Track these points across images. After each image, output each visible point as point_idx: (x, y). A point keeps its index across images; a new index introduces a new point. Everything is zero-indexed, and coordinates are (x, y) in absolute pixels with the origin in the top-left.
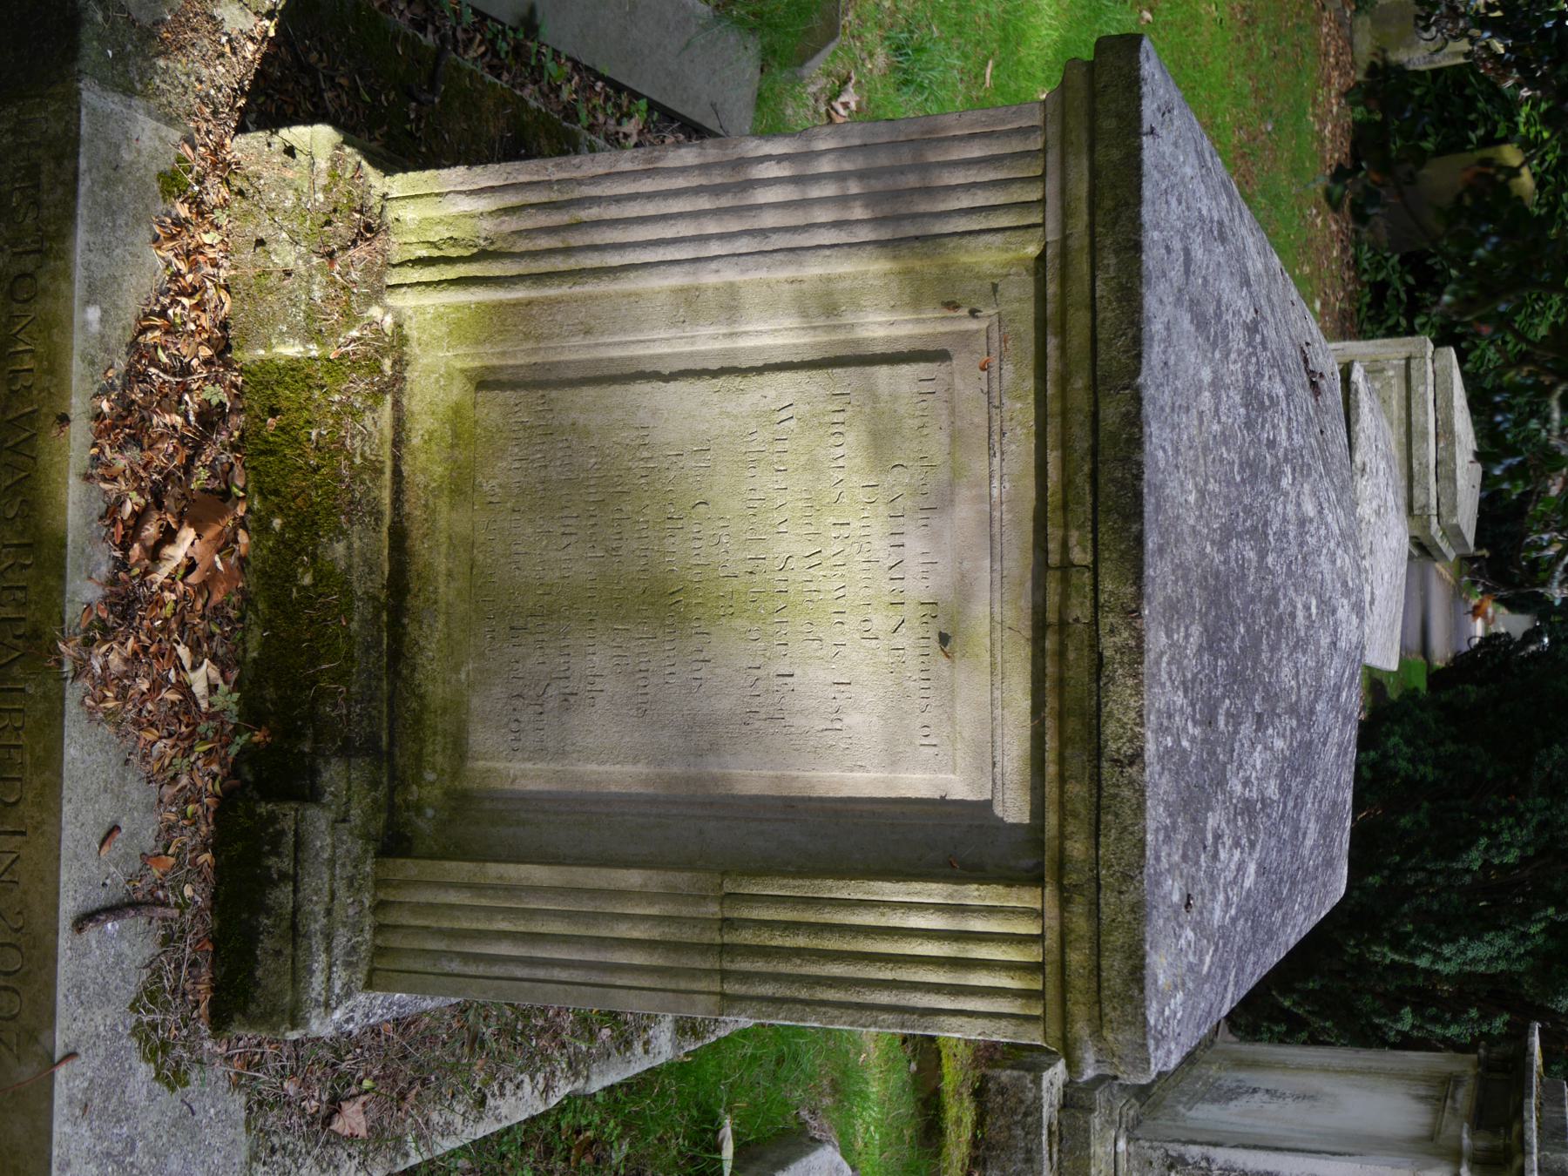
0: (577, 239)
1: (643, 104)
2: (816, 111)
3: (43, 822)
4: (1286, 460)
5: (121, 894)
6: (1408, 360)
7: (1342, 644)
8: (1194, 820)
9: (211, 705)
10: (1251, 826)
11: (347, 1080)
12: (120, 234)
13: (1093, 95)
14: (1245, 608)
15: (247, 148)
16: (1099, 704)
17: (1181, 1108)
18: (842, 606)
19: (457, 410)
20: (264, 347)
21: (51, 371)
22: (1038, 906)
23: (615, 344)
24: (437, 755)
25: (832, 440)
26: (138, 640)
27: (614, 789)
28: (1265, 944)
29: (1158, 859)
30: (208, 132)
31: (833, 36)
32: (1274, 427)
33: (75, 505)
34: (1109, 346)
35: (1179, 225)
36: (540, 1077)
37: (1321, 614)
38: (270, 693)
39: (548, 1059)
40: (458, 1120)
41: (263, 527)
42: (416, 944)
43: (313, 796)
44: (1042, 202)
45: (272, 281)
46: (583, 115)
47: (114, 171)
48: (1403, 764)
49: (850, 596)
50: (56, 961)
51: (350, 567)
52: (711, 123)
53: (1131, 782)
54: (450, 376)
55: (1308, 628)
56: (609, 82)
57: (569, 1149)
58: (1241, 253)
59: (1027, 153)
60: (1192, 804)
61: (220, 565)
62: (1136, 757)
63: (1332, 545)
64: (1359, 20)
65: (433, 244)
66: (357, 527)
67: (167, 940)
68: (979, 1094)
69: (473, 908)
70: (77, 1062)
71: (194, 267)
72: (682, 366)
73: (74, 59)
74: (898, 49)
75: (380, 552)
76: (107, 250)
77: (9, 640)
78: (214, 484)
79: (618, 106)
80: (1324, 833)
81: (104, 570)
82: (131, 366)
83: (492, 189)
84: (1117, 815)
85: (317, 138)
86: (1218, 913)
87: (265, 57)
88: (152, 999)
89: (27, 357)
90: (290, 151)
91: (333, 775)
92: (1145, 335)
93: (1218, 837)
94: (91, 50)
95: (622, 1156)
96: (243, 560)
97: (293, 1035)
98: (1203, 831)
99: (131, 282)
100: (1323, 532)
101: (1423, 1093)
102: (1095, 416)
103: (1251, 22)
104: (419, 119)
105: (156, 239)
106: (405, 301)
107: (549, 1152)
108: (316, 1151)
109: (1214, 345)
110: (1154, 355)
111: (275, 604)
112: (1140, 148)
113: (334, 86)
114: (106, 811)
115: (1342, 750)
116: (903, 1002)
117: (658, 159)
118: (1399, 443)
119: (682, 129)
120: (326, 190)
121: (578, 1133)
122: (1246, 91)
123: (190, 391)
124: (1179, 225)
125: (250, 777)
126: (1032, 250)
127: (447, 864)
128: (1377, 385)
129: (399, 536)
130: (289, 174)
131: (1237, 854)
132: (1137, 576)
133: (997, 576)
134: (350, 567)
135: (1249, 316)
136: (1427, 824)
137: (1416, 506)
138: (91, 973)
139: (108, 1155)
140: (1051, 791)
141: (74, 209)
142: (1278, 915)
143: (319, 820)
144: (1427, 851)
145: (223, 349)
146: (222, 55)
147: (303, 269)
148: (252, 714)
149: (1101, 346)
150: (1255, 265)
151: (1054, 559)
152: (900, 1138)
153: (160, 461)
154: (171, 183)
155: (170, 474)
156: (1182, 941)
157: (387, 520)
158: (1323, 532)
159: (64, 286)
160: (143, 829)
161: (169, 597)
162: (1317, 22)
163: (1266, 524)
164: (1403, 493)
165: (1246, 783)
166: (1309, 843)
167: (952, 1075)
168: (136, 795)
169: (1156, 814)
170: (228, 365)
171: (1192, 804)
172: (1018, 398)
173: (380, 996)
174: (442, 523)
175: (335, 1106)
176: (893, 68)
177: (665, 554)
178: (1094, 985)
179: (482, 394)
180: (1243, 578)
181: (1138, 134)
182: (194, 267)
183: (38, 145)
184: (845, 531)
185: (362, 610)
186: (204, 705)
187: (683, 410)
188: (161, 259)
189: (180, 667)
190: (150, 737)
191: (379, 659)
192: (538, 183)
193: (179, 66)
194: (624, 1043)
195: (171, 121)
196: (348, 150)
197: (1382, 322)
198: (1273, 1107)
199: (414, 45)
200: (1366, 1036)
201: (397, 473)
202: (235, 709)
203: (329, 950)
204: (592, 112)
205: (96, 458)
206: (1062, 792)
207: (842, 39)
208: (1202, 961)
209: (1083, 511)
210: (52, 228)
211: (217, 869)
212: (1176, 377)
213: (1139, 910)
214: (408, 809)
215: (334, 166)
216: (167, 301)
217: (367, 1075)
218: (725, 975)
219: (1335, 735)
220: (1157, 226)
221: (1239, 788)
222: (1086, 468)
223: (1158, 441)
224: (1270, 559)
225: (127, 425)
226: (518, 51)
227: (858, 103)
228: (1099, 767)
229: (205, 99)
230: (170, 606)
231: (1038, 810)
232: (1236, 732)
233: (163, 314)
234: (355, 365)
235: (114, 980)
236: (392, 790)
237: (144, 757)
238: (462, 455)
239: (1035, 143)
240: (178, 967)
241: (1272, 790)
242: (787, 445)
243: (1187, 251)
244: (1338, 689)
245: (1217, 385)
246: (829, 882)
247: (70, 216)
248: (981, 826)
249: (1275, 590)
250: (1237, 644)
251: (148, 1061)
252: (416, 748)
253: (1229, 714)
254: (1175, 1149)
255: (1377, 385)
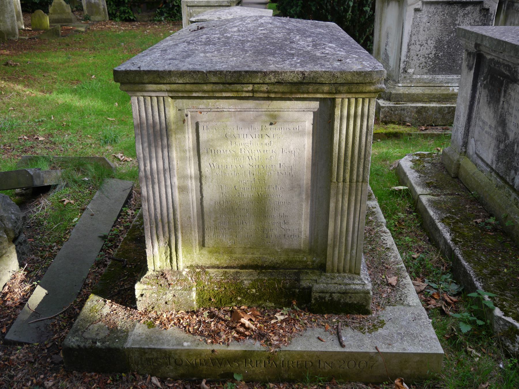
0: (166, 220)
1: (124, 209)
2: (123, 164)
3: (317, 356)
4: (223, 35)
5: (335, 336)
6: (188, 6)
7: (271, 21)
8: (318, 59)
9: (286, 315)
10: (319, 45)
11: (383, 282)
12: (164, 338)
13: (130, 83)
14: (262, 45)
15: (141, 306)
16: (289, 83)
17: (390, 69)
18: (264, 149)
19: (210, 252)
20: (193, 302)
21: (201, 355)
22: (341, 99)
23: (193, 210)
24: (300, 257)
25: (219, 153)
26: (270, 333)
27: (309, 211)
28: (349, 42)
29: (329, 68)
30: (137, 316)
31: (104, 159)
32: (214, 38)
33: (235, 347)
34: (195, 79)
35: (163, 61)
36: (382, 234)
37: (263, 26)
38: (283, 300)
39: (377, 232)
40: (393, 254)
41: (240, 302)
42: (348, 262)
43: (310, 289)
44: (157, 97)
45: (176, 300)
46: (127, 224)
47: (149, 338)
48: (298, 9)
49: (260, 148)
50: (352, 352)
51: (251, 280)
52: (128, 191)
53: (309, 74)
54: (201, 254)
55: (267, 30)
56: (118, 217)
57: (400, 228)
58: (168, 46)
59: (144, 101)
60: (314, 59)
61: (250, 313)
62: (303, 73)
63: (244, 23)
64: (92, 19)
65: (166, 258)
66: (240, 278)
67: (347, 325)
68: (386, 123)
69: (339, 247)
70: (378, 347)
71: (172, 319)
72: (199, 193)
73: (119, 349)
74: (106, 143)
75: (247, 272)
76: (169, 341)
77: (270, 365)
78: (229, 314)
79: (124, 215)
80: (320, 27)
81: (252, 341)
82: (199, 335)
83: (152, 242)
84: (318, 78)
85: (139, 288)
86: (342, 53)
87: (116, 303)
88: (362, 329)
89: (197, 361)
90: (142, 295)
91: (305, 283)
92: (193, 70)
93: (323, 53)
94: (117, 344)
95: (402, 215)
96: (248, 308)
97: (371, 293)
98: (321, 57)
99: (177, 335)
100: (241, 26)
101: (387, 4)
102: (214, 83)
103: (94, 49)
104: (131, 265)
105: (165, 329)
106: (181, 265)
107: (401, 233)
108: (401, 289)
109: (194, 53)
110: (198, 68)
111: (260, 299)
112: (144, 71)
113: (123, 285)
114: (314, 340)
115: (298, 22)
116: (365, 135)
117: (145, 198)
118: (211, 9)
119: (130, 199)
120: (152, 286)
121: (396, 226)
122: (113, 50)
123: (205, 321)
124: (163, 61)
125: (305, 305)
126: (170, 100)
127: (328, 254)
128: (195, 15)
129: (243, 267)
130: (148, 295)
131: (327, 48)
132: (255, 73)
133: (255, 110)
134: (251, 280)
135: (186, 44)
136: (314, 3)
137: (227, 5)
138: (355, 343)
139: (401, 339)
140: (311, 96)
141: (158, 349)
142: (342, 39)
143: (316, 287)
144: (322, 2)
145: (193, 312)
146: (116, 313)
147: (173, 292)
148: (289, 304)
149: (196, 81)
150: (171, 43)
151: (251, 95)
152: (398, 144)
153: (223, 328)
154: (151, 325)
155: (227, 325)
156: (350, 62)
157: (238, 270)
158: (241, 26)
159: (178, 351)
160: (319, 331)
161: (258, 325)
162: (93, 30)
163: (240, 40)
164: (224, 8)
165: (308, 46)
166: (323, 31)
167: (382, 130)
168: (310, 333)
169: (317, 68)
170: (198, 311)
171: (314, 59)
172: (209, 104)
173: (361, 272)
174: (239, 256)
175: (389, 285)
176: (111, 144)
177: (248, 197)
178: (361, 85)
179: (206, 245)
180: (254, 46)
181: (140, 71)
182: (172, 319)
183: (141, 359)
184: (243, 150)
185: (262, 277)
186: (286, 317)
187: (211, 193)
188: (171, 328)
189: (277, 322)
190: (295, 330)
191: (275, 272)
192: (151, 230)
193: (120, 324)
194: (373, 213)
195: (134, 326)
196: (141, 280)
197: (176, 14)
198: (390, 44)
199: (111, 266)
200: (371, 20)
201: (226, 268)
202: (287, 309)
203: (350, 284)
204: (126, 222)
205: (223, 343)
206: (311, 93)
207: (104, 156)
208: (355, 57)
209: (239, 87)
210: (163, 355)
211: (328, 313)
212: (203, 62)
213: (342, 72)
214: (313, 264)
215: (146, 284)
216: (181, 327)
217: (381, 277)
218: (357, 181)
219: (295, 24)
220: (164, 67)
221: (310, 48)
222: (227, 86)
223: (219, 67)
224: (249, 39)
225: (214, 335)
226: (111, 241)
227: (121, 153)
228: (305, 83)
229: (128, 317)
230: (261, 325)
231: (316, 99)
232: (295, 48)
233: (185, 327)
234: (198, 278)
235: (357, 338)
236: (308, 269)
237: (300, 331)
238: (222, 251)
239: (142, 99)
240: (354, 323)
241: (310, 39)
242: (220, 165)
243: (170, 59)
244: (282, 22)
245: (205, 52)
246: (334, 154)
247: (160, 350)
248: (320, 115)
249: (258, 38)
250: (272, 48)
251: (378, 330)
252: (298, 263)
253: (291, 50)
254: (401, 70)
255: (195, 15)
